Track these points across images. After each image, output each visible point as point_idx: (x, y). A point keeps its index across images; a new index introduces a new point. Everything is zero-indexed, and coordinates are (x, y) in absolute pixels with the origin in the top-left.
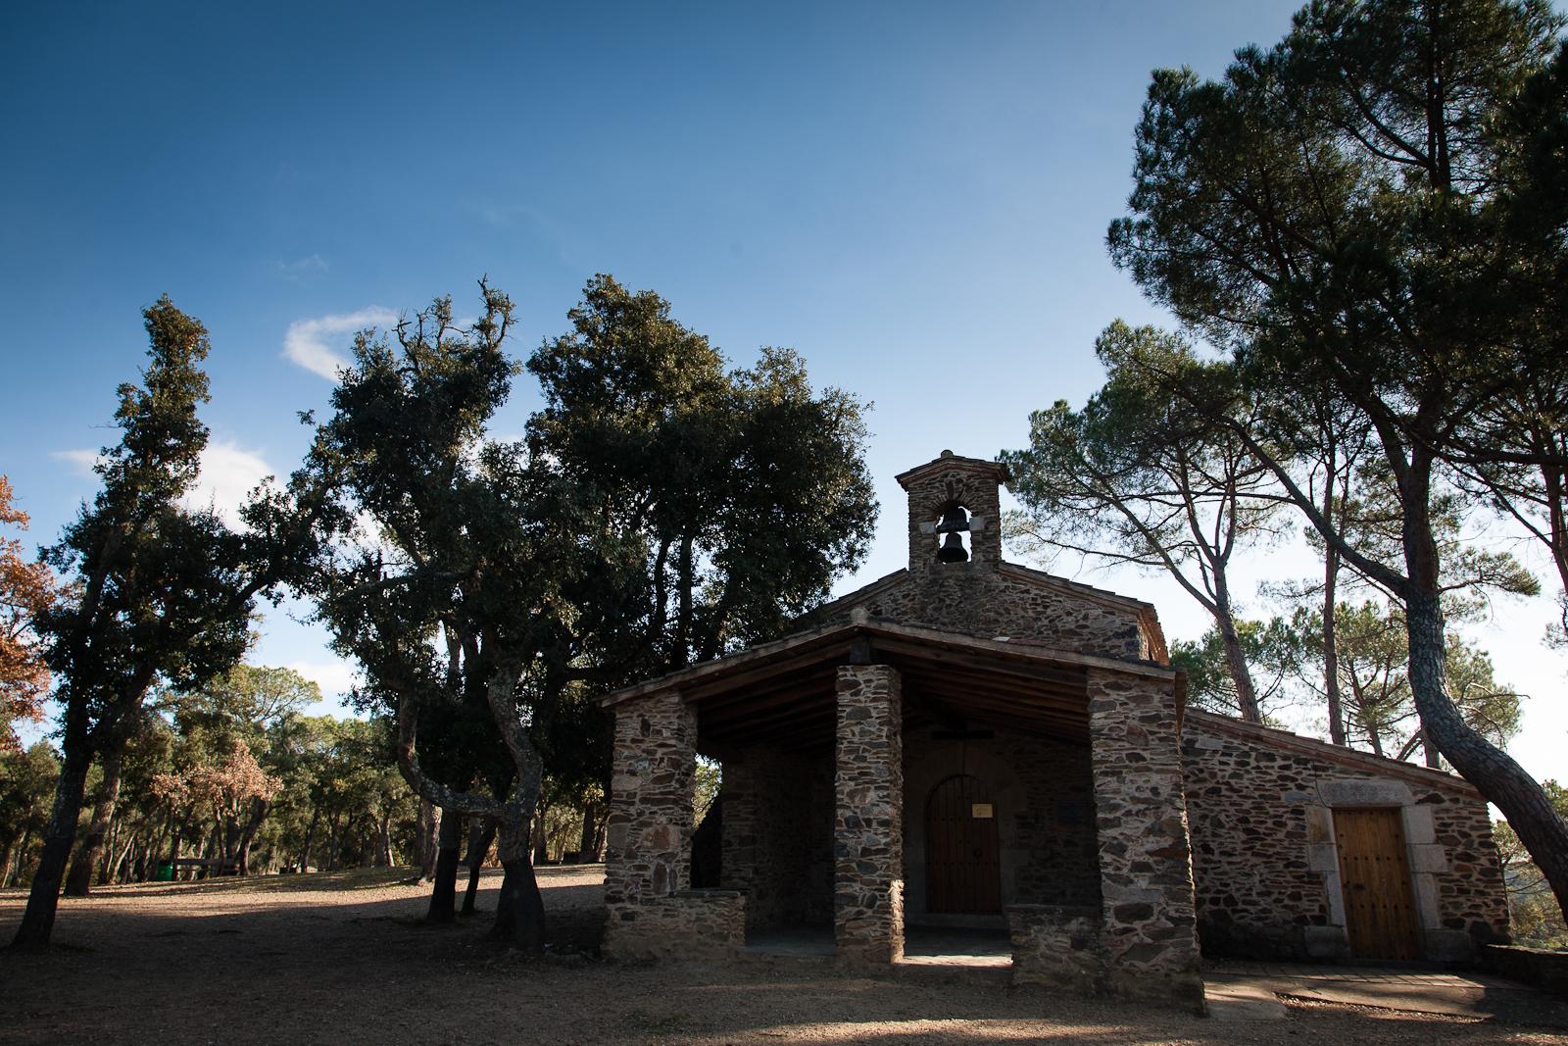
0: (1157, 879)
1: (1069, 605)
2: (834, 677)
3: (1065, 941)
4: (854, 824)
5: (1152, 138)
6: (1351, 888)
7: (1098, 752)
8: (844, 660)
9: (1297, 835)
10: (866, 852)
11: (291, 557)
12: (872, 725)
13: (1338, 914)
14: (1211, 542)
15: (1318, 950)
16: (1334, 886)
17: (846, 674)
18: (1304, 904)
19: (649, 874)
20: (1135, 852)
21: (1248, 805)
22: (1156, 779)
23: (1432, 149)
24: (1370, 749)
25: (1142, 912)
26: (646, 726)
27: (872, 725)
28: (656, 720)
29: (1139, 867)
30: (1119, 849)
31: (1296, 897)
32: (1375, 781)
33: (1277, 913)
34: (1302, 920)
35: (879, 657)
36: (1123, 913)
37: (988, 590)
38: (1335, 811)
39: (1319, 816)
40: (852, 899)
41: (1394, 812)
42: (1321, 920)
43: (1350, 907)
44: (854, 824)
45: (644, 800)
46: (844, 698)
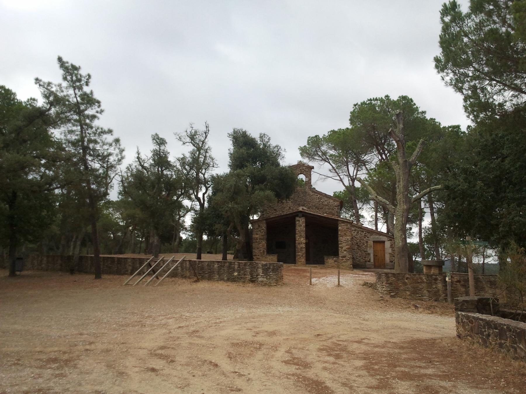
0: (348, 252)
1: (326, 199)
2: (295, 219)
3: (333, 261)
4: (299, 244)
5: (419, 252)
6: (375, 256)
7: (339, 233)
8: (297, 216)
9: (367, 246)
10: (301, 248)
11: (44, 165)
12: (302, 227)
13: (372, 260)
14: (352, 175)
15: (367, 266)
16: (372, 256)
17: (297, 218)
18: (366, 259)
19: (262, 252)
20: (344, 248)
21: (358, 241)
22: (348, 237)
23: (425, 195)
24: (374, 228)
25: (345, 257)
26: (259, 226)
27: (302, 227)
28: (261, 225)
29: (345, 250)
30: (342, 248)
31: (365, 257)
32: (381, 237)
33: (362, 260)
34: (366, 261)
35: (303, 216)
36: (342, 257)
37: (309, 195)
38: (374, 242)
39: (371, 243)
40: (299, 255)
41: (384, 242)
42: (369, 261)
43: (374, 259)
44: (299, 244)
45: (260, 239)
46: (297, 222)
